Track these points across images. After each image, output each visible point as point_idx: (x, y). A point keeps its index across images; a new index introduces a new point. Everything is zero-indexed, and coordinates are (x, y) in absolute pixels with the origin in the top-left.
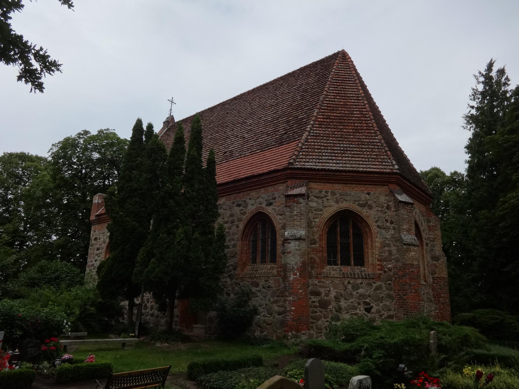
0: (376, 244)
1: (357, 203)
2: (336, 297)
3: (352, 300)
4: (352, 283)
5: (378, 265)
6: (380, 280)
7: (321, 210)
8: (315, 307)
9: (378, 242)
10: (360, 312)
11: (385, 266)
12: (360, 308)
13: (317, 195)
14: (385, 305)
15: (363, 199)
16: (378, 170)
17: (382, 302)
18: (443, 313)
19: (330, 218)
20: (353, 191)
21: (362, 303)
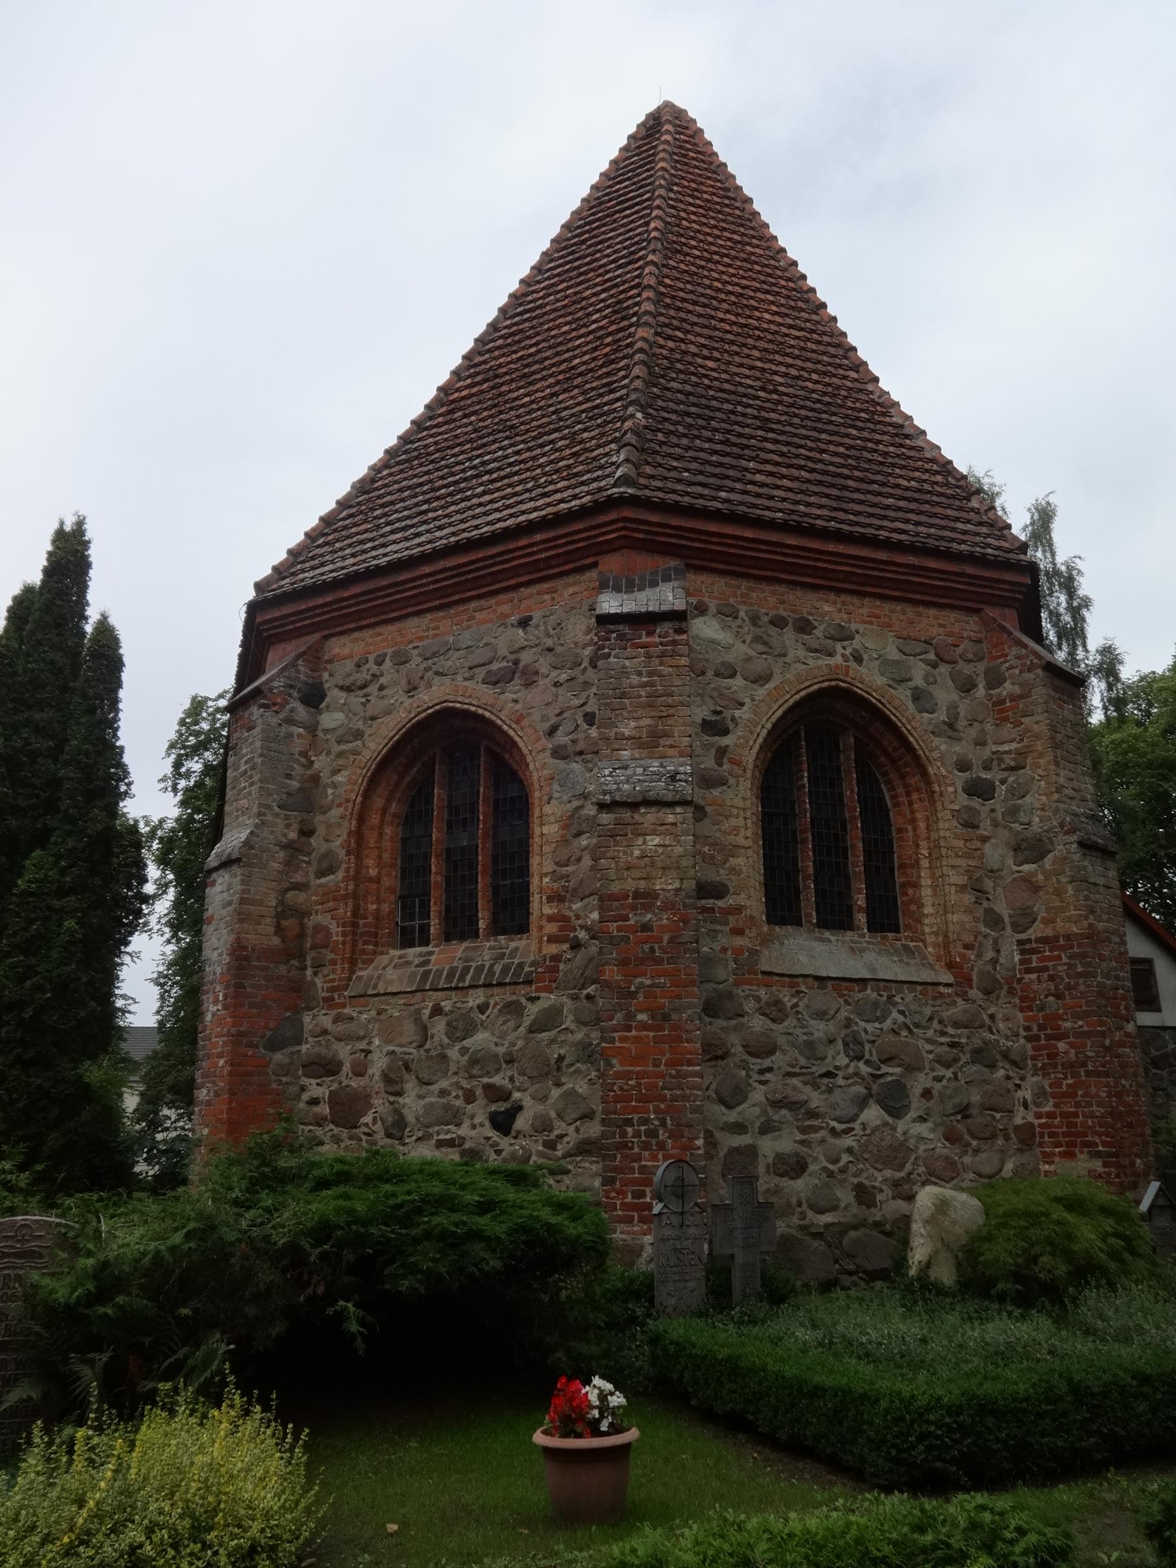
0: (546, 829)
1: (481, 673)
2: (387, 1078)
3: (444, 1084)
4: (451, 1012)
5: (550, 919)
6: (554, 985)
7: (359, 735)
8: (319, 1121)
9: (552, 819)
10: (473, 1133)
11: (578, 917)
12: (472, 1117)
13: (347, 682)
14: (572, 1093)
15: (503, 651)
17: (558, 1084)
18: (1076, 1115)
20: (469, 627)
21: (479, 1092)
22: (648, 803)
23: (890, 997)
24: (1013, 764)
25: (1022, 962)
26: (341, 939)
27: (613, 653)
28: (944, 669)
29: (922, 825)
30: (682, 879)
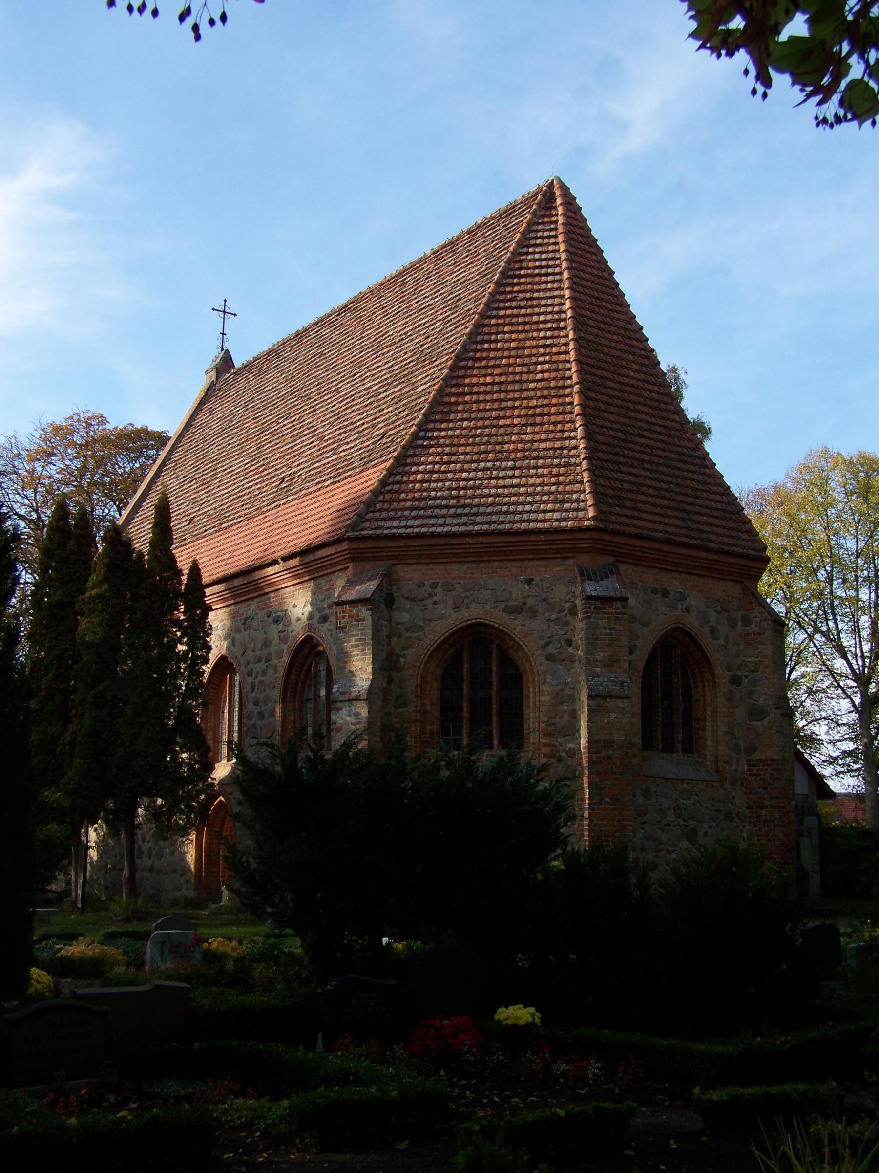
0: (542, 698)
1: (502, 606)
5: (545, 745)
7: (422, 628)
16: (547, 525)
19: (438, 645)
22: (611, 697)
23: (693, 787)
24: (752, 669)
25: (748, 770)
26: (414, 745)
27: (593, 616)
28: (724, 614)
29: (708, 698)
30: (626, 735)
